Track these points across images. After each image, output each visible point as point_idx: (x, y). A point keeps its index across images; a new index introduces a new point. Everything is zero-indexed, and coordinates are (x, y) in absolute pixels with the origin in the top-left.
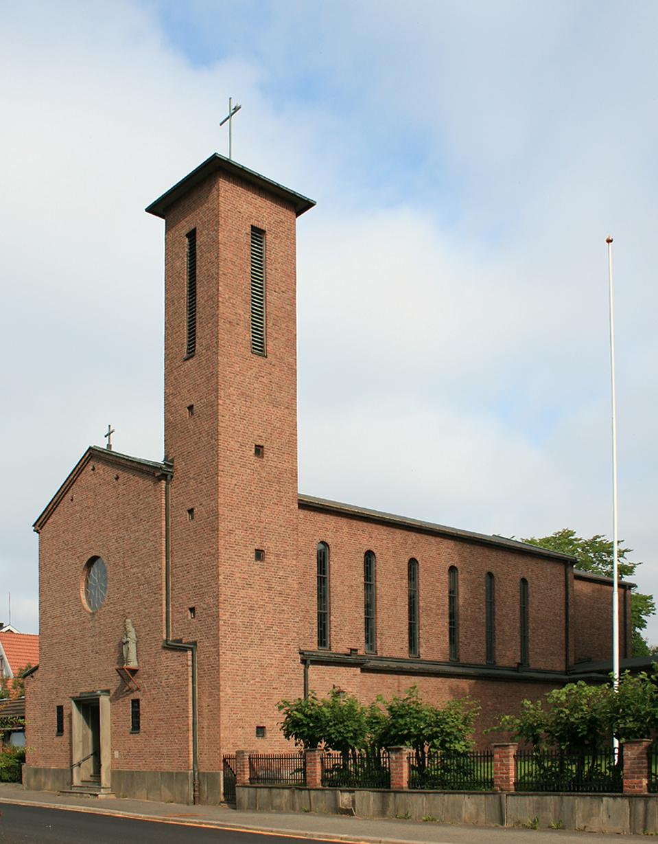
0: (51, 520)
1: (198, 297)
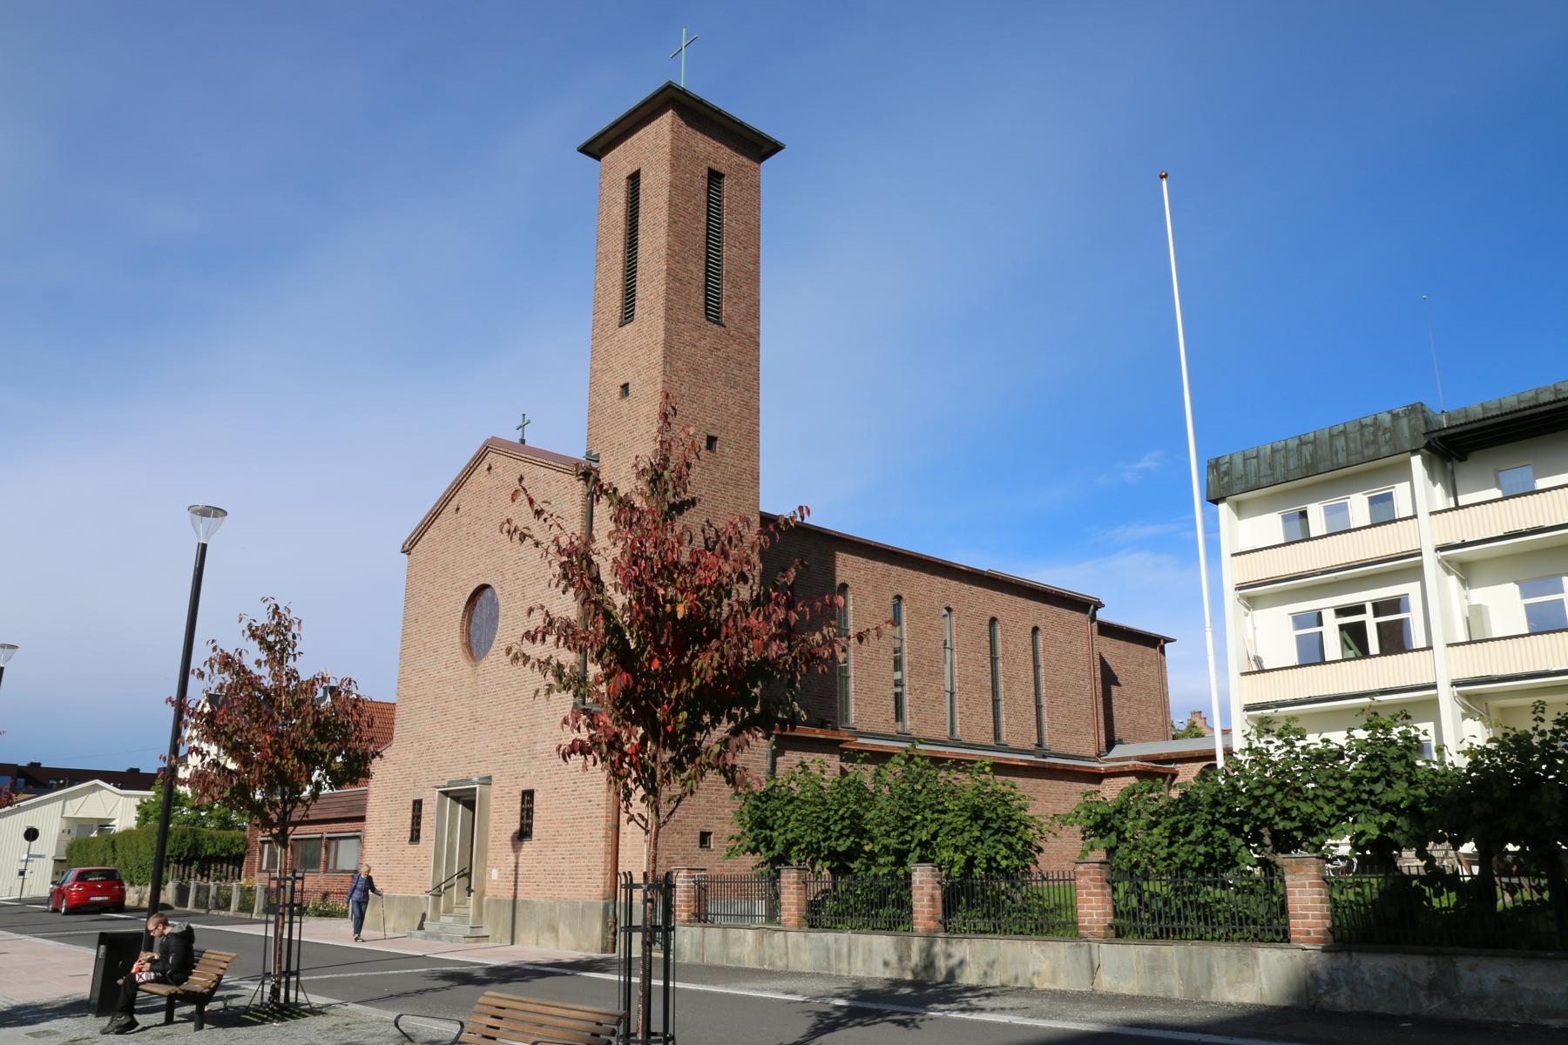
0: (426, 536)
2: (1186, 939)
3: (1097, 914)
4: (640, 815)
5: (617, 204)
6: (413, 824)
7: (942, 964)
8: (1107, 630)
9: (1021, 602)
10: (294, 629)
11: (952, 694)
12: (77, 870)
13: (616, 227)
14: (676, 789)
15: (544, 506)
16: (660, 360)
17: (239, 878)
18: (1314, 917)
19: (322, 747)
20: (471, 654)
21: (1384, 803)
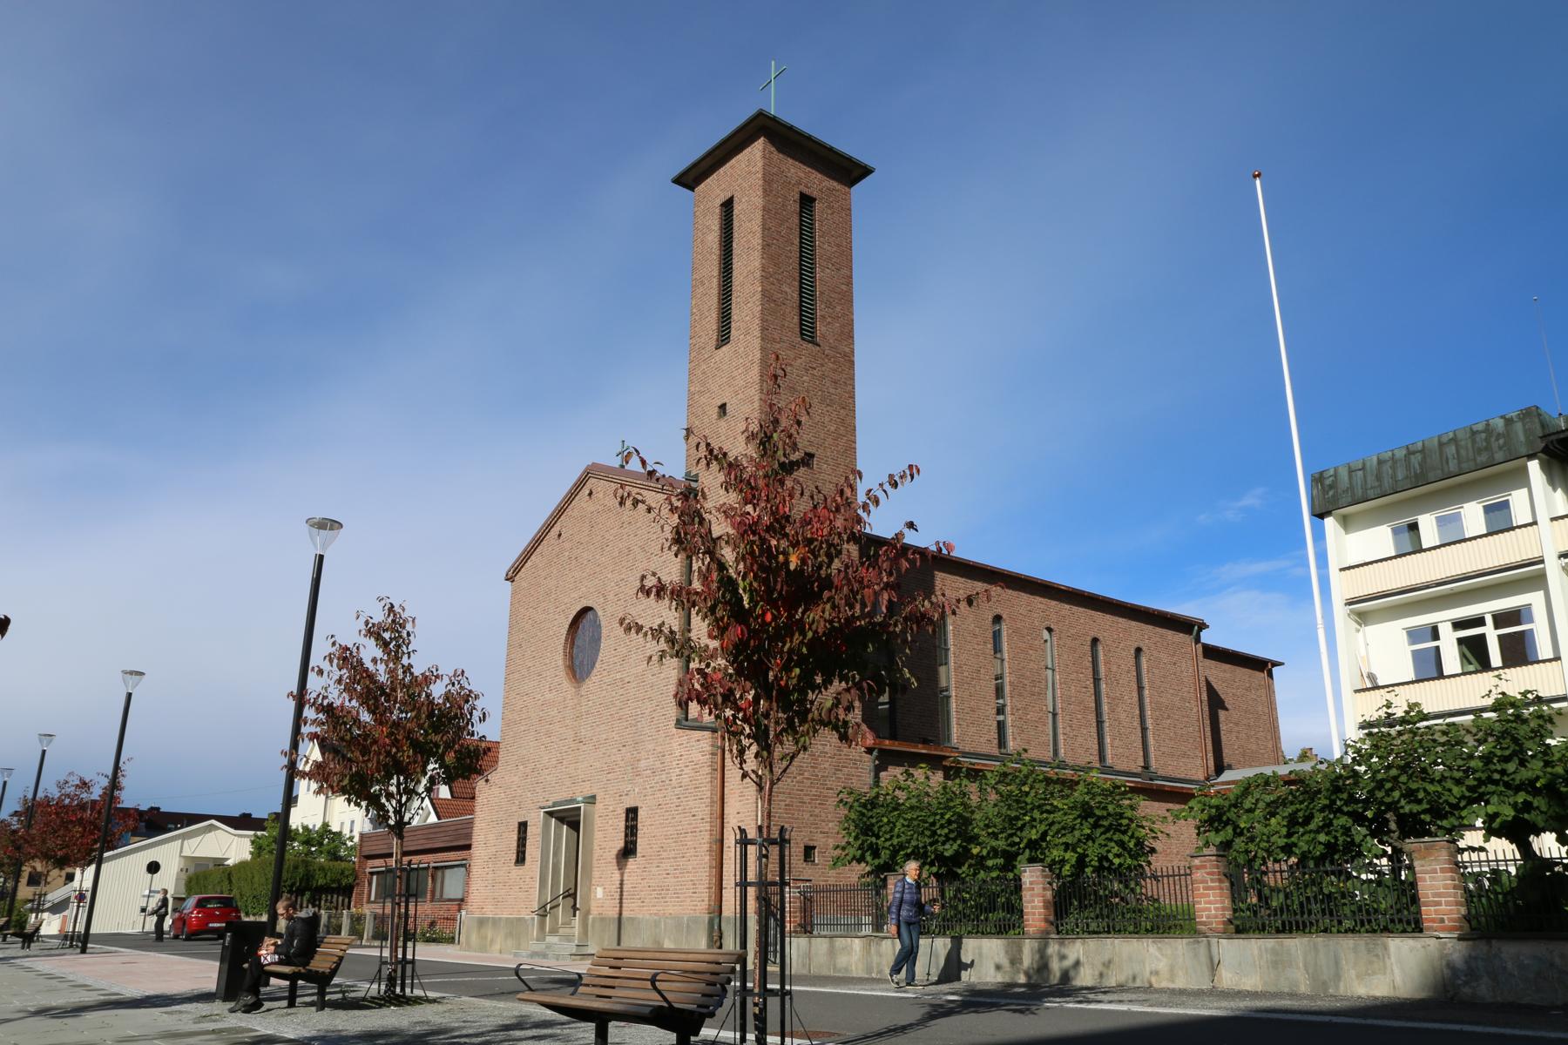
1: (735, 274)
2: (1310, 932)
3: (1216, 909)
4: (753, 771)
5: (711, 230)
6: (518, 846)
7: (1056, 967)
8: (1212, 653)
9: (1123, 622)
10: (409, 627)
11: (1055, 715)
12: (197, 896)
13: (711, 254)
14: (789, 745)
15: (656, 467)
16: (757, 378)
17: (349, 908)
18: (1447, 904)
19: (437, 738)
20: (574, 676)
21: (1517, 782)
